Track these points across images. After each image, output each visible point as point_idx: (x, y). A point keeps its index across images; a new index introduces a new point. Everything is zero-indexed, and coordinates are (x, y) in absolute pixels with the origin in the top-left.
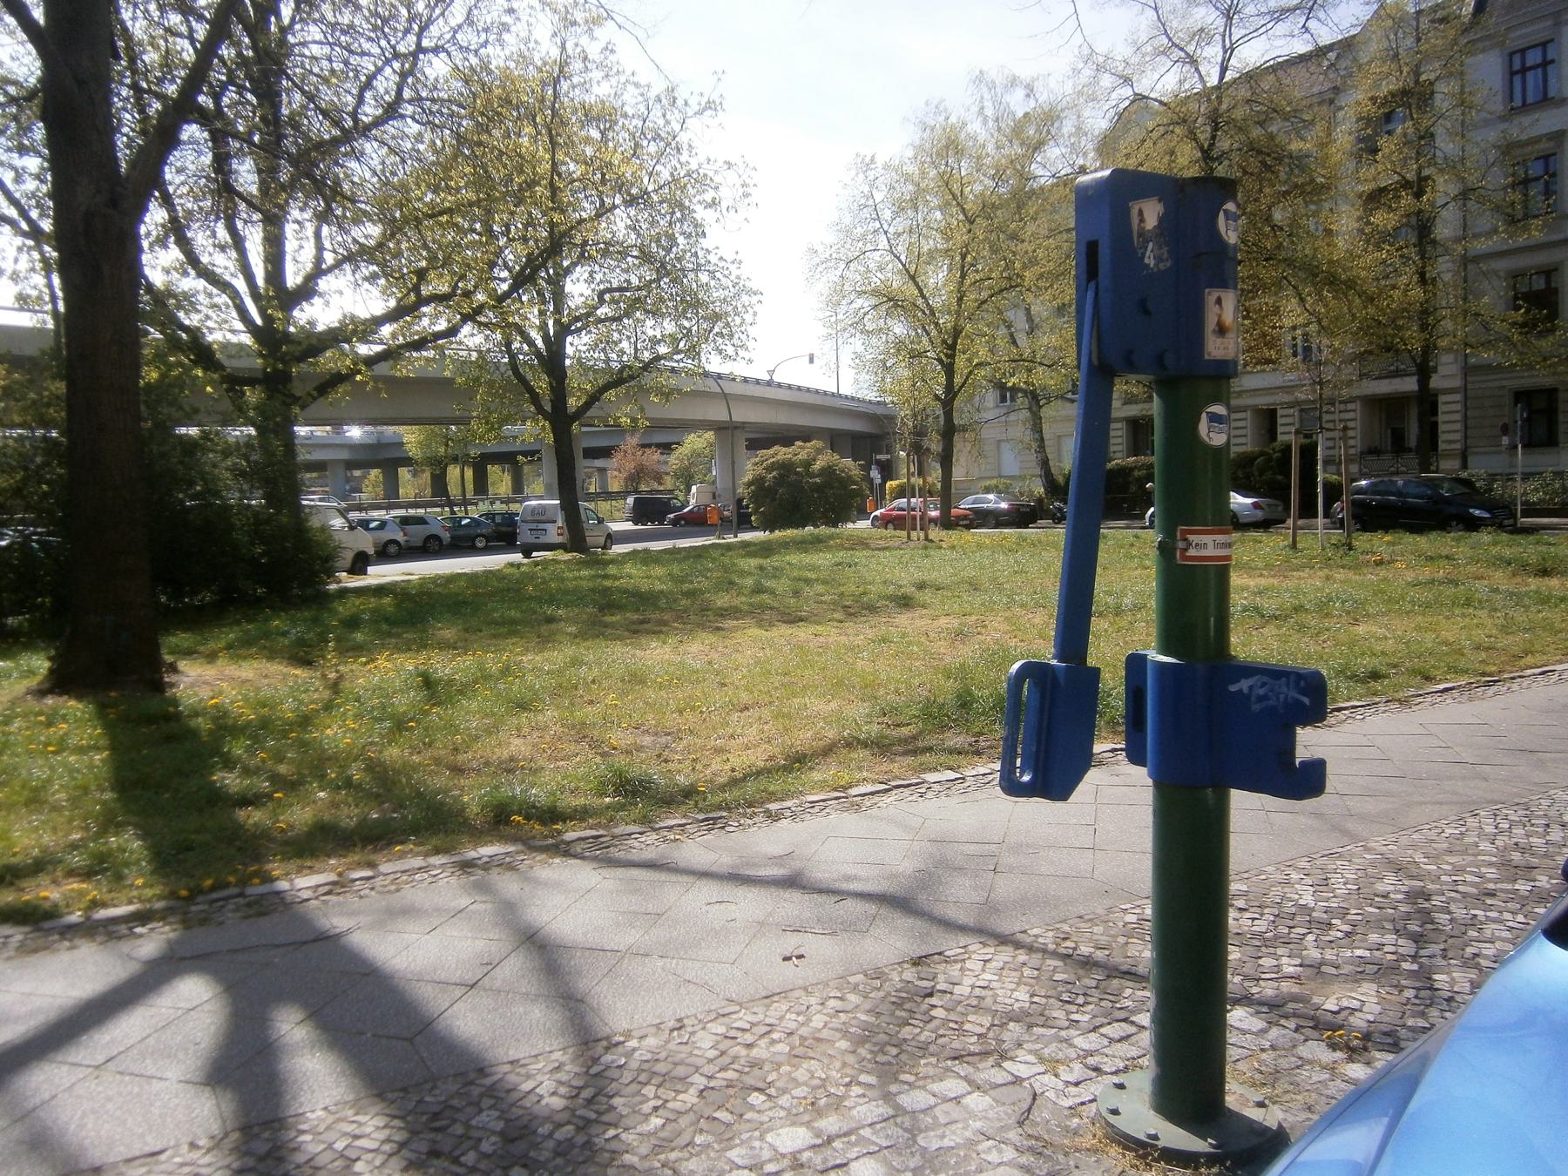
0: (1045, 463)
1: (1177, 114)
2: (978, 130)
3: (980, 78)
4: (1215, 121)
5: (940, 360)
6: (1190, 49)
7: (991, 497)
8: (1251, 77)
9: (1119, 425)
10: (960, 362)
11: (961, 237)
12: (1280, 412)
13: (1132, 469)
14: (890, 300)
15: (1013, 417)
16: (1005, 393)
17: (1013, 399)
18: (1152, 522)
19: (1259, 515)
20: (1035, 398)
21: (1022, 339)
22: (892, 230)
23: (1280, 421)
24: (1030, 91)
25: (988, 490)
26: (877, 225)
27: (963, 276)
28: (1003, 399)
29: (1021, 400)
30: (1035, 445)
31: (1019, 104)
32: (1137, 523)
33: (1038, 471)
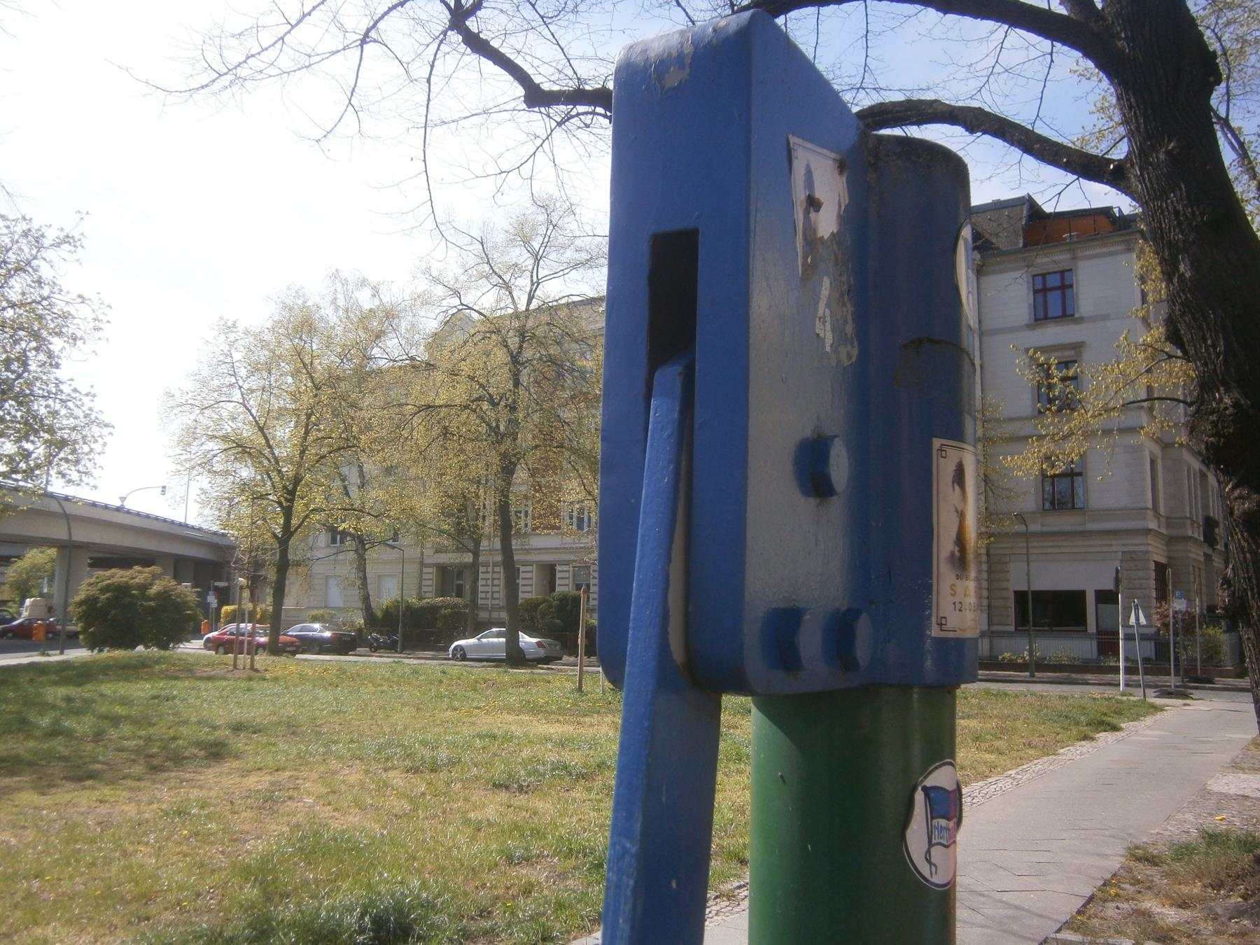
0: (366, 599)
1: (493, 327)
2: (330, 316)
3: (335, 275)
4: (522, 334)
5: (280, 503)
6: (507, 278)
7: (317, 626)
8: (550, 309)
9: (430, 570)
10: (299, 506)
11: (307, 400)
12: (558, 568)
13: (440, 608)
14: (239, 446)
15: (341, 557)
16: (336, 535)
17: (342, 542)
18: (454, 655)
19: (542, 653)
20: (362, 542)
21: (354, 492)
22: (246, 386)
23: (558, 575)
24: (376, 292)
25: (315, 619)
26: (233, 380)
27: (307, 433)
28: (334, 541)
29: (349, 542)
30: (358, 582)
31: (366, 301)
32: (442, 655)
33: (360, 605)
